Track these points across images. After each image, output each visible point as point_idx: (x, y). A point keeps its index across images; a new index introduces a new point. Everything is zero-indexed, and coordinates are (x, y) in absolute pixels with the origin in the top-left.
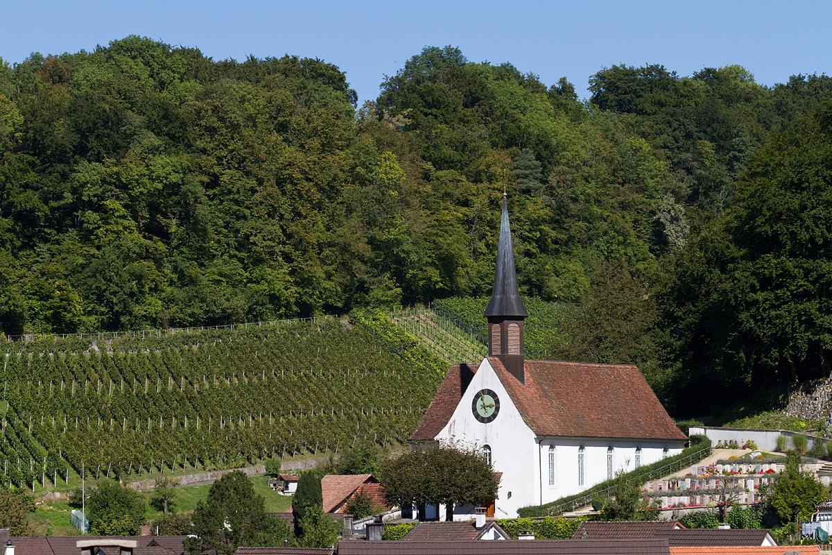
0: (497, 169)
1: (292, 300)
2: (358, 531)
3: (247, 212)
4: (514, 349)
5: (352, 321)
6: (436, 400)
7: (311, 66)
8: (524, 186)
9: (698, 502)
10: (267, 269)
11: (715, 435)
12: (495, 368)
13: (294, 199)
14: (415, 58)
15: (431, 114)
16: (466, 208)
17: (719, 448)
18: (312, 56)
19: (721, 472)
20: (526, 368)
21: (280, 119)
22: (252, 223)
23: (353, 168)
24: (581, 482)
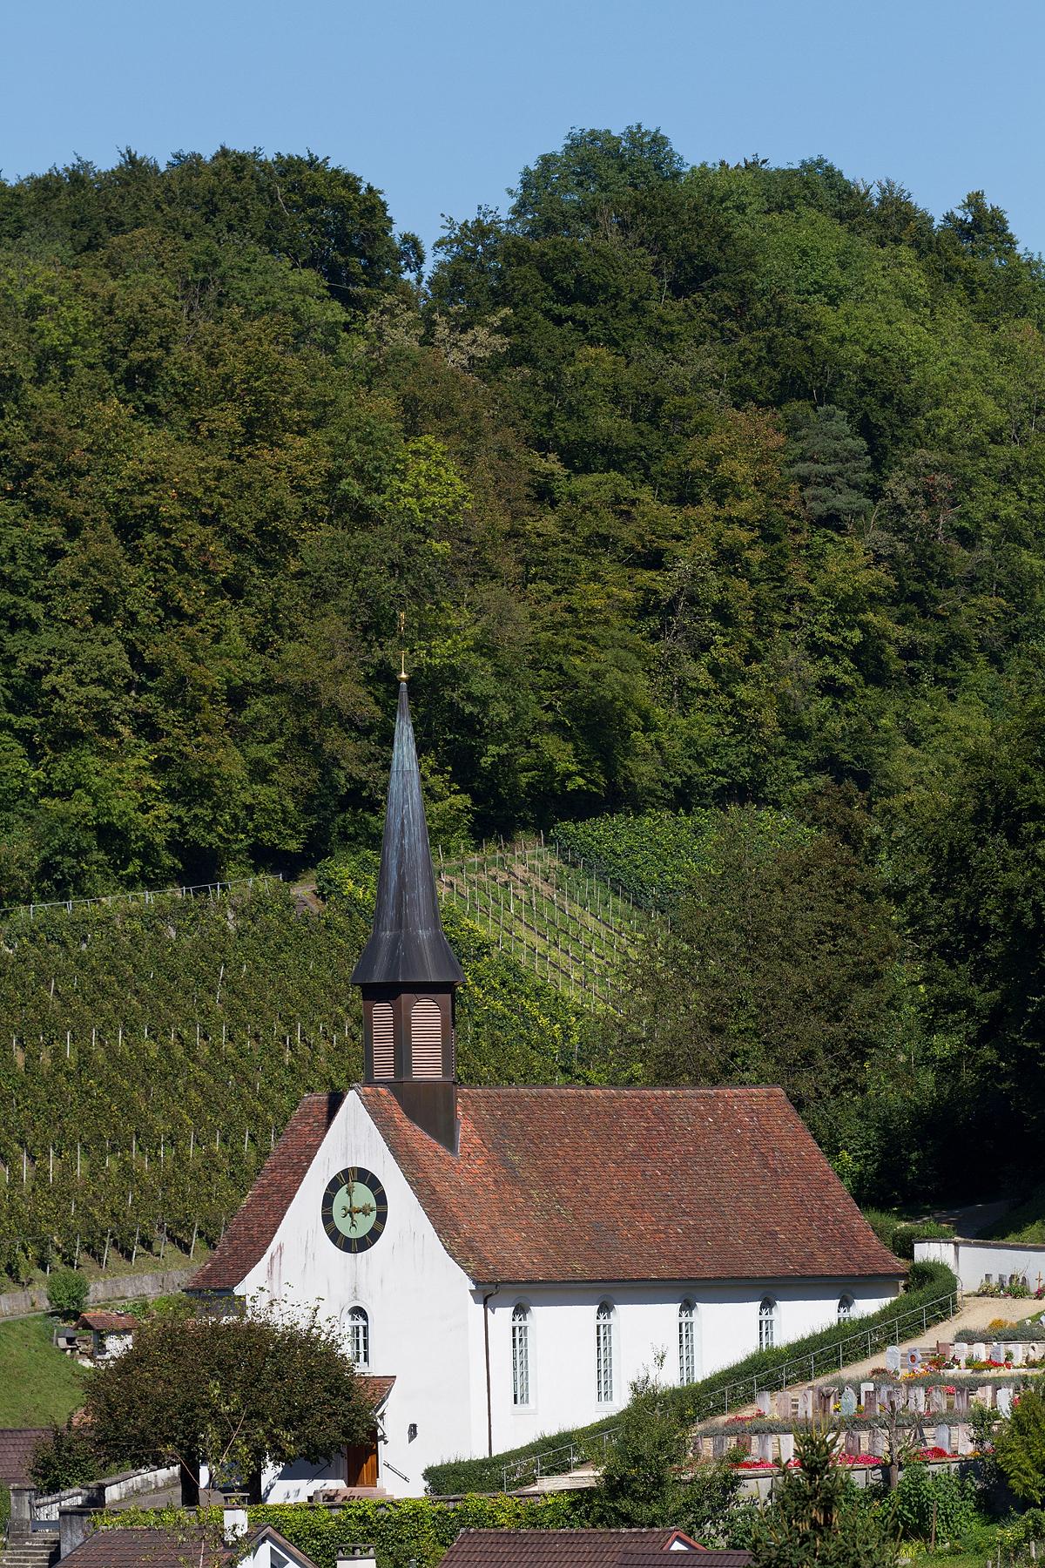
0: (739, 469)
1: (160, 839)
2: (48, 1524)
3: (37, 610)
4: (427, 1066)
5: (322, 889)
6: (262, 1186)
7: (292, 177)
8: (819, 508)
9: (865, 1447)
10: (91, 759)
11: (969, 1263)
12: (374, 1114)
13: (165, 571)
14: (547, 161)
15: (571, 318)
16: (652, 574)
17: (984, 1294)
18: (296, 148)
19: (963, 1364)
20: (465, 1109)
21: (137, 356)
22: (48, 639)
23: (333, 478)
24: (604, 1393)
